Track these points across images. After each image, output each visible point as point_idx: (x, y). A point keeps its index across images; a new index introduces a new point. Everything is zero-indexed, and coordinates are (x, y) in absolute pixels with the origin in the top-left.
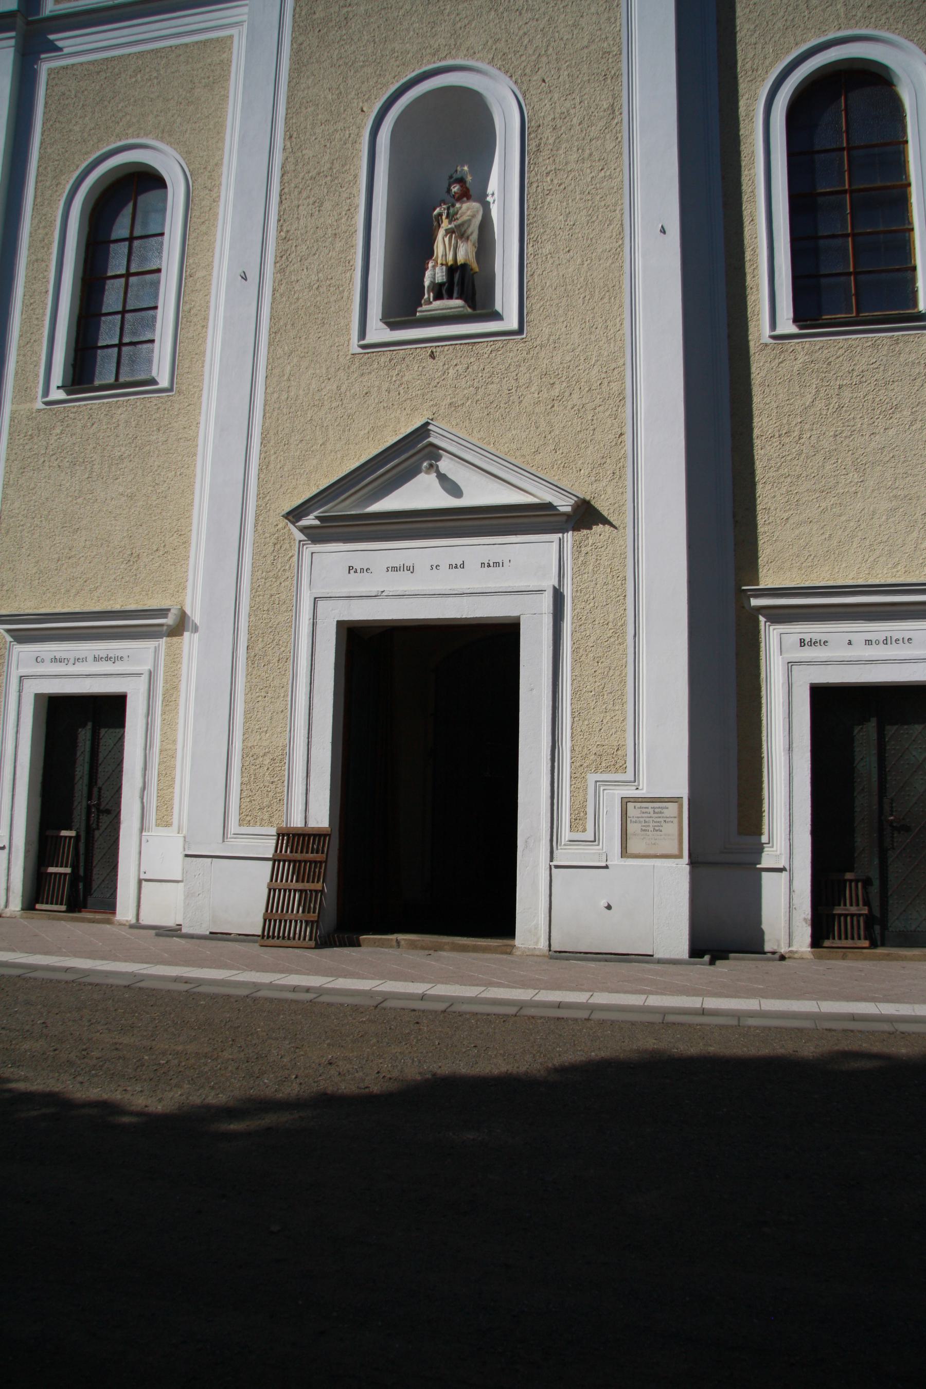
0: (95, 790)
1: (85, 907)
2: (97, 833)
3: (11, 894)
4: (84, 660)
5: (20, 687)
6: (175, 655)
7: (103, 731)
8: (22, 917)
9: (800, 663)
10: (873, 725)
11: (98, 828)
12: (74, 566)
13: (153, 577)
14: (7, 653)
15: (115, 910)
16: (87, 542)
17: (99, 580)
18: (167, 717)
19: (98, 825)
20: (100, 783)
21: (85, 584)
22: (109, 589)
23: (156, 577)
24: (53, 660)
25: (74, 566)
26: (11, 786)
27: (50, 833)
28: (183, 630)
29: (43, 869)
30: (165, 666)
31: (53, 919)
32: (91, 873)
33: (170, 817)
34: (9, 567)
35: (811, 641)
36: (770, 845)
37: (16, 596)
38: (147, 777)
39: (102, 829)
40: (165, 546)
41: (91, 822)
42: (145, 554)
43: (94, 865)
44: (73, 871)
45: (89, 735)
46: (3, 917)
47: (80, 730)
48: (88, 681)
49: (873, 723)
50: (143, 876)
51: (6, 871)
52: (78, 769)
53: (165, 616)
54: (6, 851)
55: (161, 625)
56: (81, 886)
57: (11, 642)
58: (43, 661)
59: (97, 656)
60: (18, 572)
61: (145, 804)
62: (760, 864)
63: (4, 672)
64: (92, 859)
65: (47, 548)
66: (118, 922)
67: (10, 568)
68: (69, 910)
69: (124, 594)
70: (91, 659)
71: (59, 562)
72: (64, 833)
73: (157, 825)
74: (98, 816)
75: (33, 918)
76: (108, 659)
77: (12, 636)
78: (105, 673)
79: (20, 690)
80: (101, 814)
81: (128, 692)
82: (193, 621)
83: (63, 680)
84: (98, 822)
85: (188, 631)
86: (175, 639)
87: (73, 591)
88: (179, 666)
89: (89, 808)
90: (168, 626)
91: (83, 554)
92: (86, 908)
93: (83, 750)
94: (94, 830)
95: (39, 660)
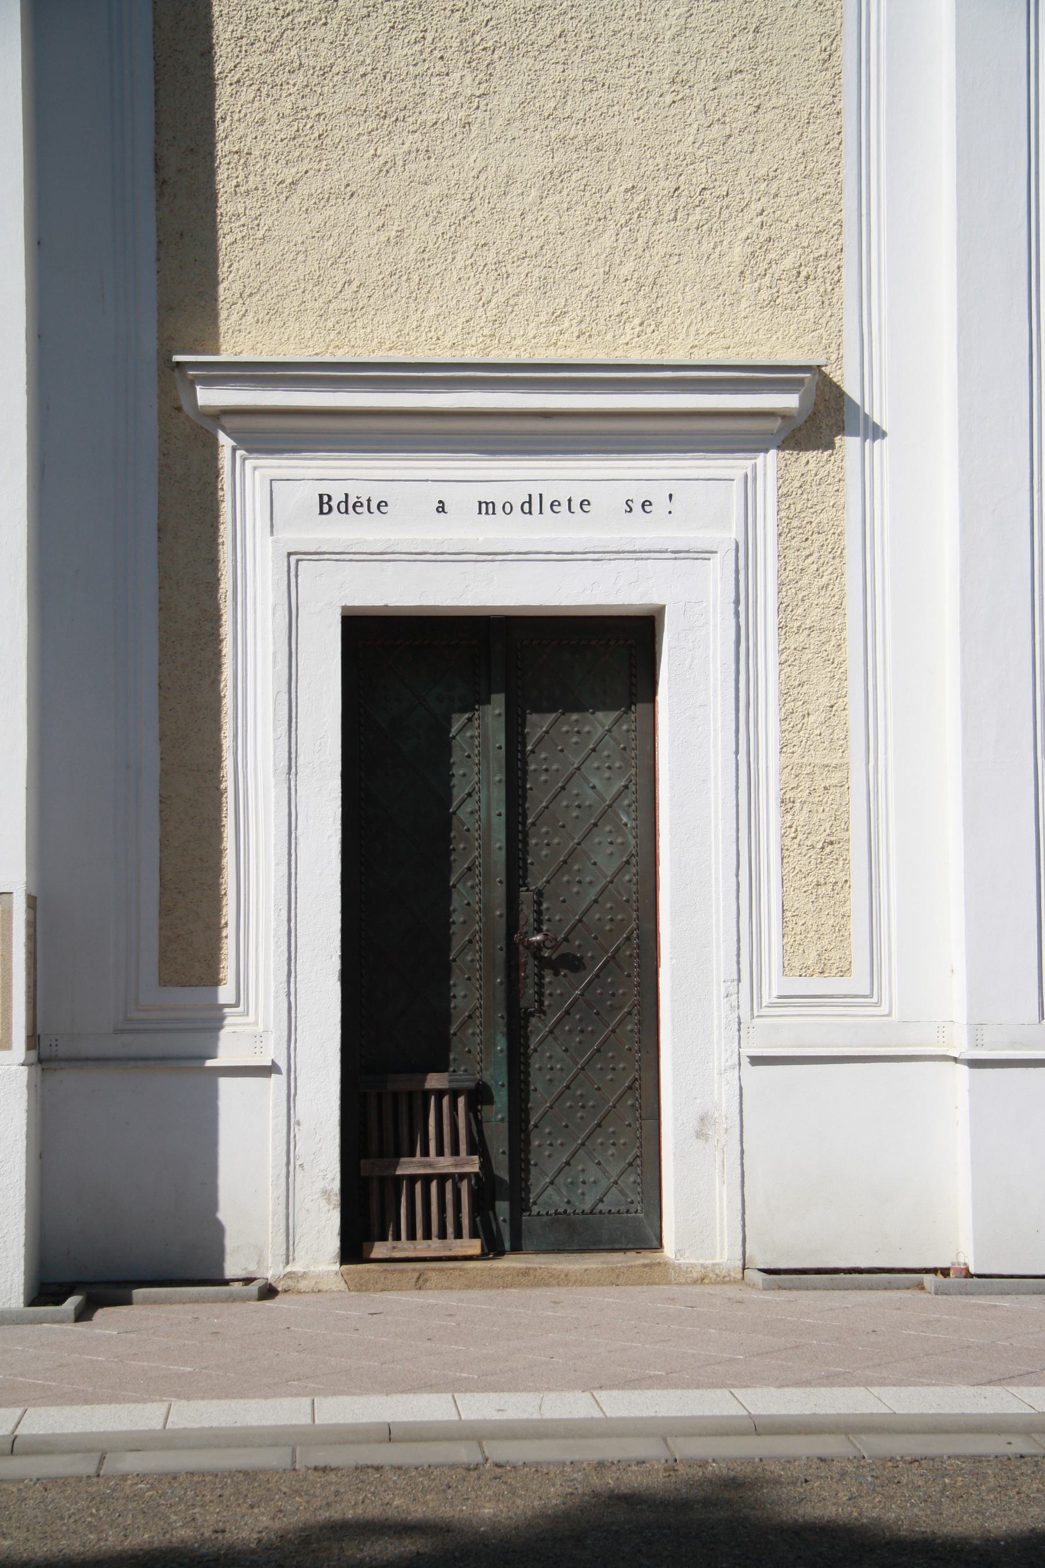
7: (538, 724)
20: (537, 879)
36: (241, 1009)
49: (495, 709)
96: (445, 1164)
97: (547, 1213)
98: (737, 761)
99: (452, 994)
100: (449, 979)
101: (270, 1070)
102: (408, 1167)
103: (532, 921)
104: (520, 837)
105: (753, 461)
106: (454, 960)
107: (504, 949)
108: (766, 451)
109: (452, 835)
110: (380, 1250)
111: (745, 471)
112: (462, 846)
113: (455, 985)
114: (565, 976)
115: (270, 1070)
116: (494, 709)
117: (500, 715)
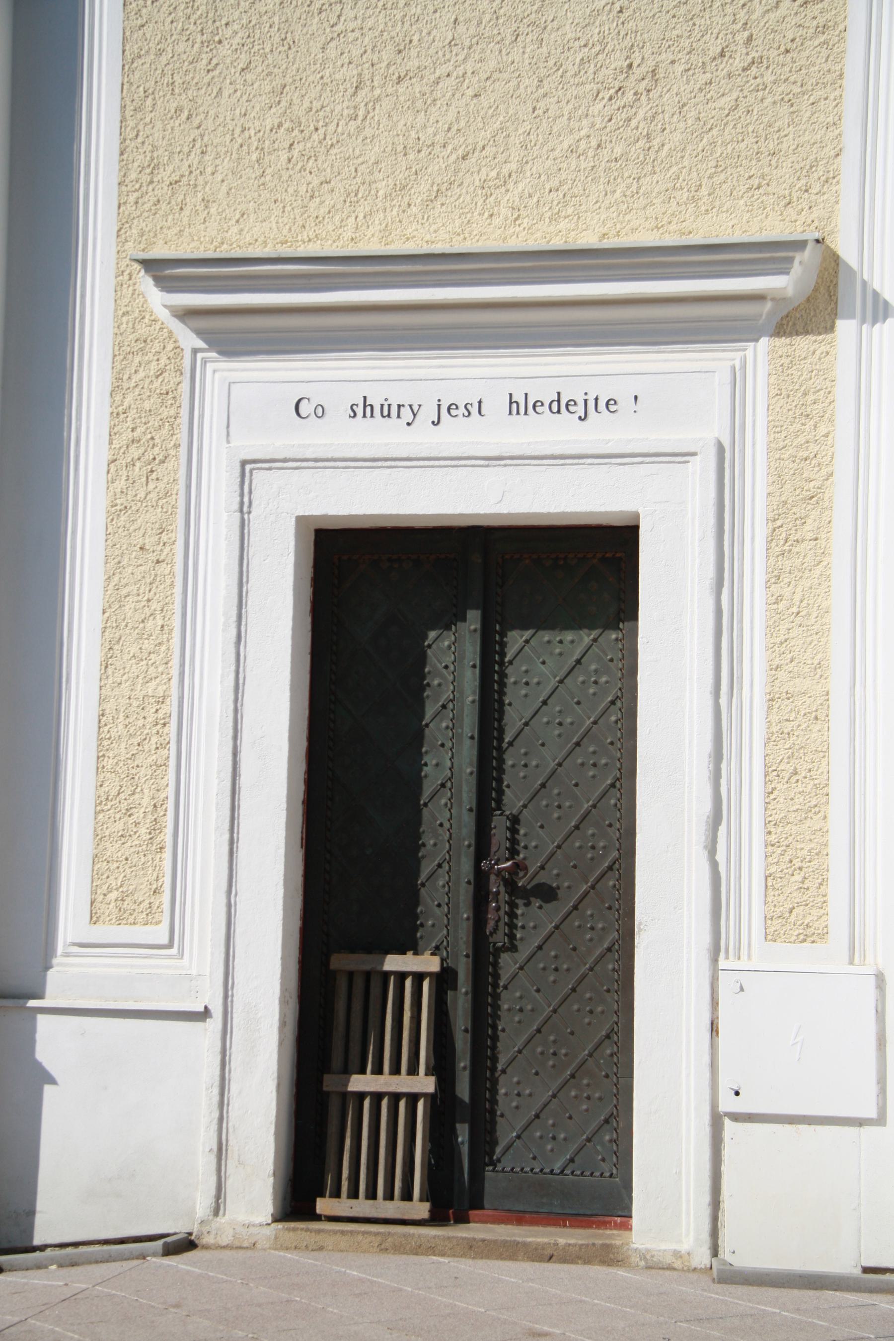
0: (499, 825)
1: (477, 1203)
2: (508, 964)
3: (231, 1166)
4: (474, 410)
5: (242, 495)
6: (805, 394)
7: (516, 639)
8: (276, 1241)
9: (269, 463)
10: (472, 627)
11: (513, 948)
12: (419, 104)
13: (713, 143)
14: (185, 387)
15: (630, 1210)
16: (461, 28)
17: (515, 154)
18: (787, 592)
19: (512, 937)
20: (513, 800)
21: (464, 165)
22: (554, 183)
23: (725, 144)
24: (359, 411)
25: (419, 104)
26: (228, 813)
27: (341, 962)
28: (834, 315)
29: (330, 1083)
30: (774, 427)
31: (399, 1249)
32: (494, 1091)
33: (815, 912)
34: (173, 105)
35: (559, 401)
36: (174, 951)
37: (206, 203)
38: (723, 781)
39: (524, 952)
40: (750, 39)
41: (491, 925)
42: (679, 68)
43: (500, 1067)
44: (440, 1083)
45: (471, 650)
46: (206, 1247)
47: (432, 634)
48: (494, 475)
49: (474, 619)
50: (728, 1104)
51: (216, 1091)
52: (430, 760)
53: (782, 267)
54: (214, 1024)
55: (757, 297)
56: (463, 1133)
57: (195, 351)
58: (321, 412)
59: (519, 398)
60: (209, 124)
61: (722, 869)
62: (40, 996)
63: (177, 446)
64: (494, 1048)
65: (315, 48)
66: (643, 1257)
67: (179, 110)
68: (437, 1218)
69: (610, 199)
70: (496, 405)
71: (362, 93)
72: (393, 963)
73: (770, 937)
74: (513, 905)
75: (321, 1248)
76: (559, 405)
77: (199, 333)
78: (557, 451)
79: (242, 503)
80: (520, 902)
81: (641, 511)
82: (864, 283)
83: (401, 475)
84: (512, 926)
85: (851, 316)
86: (803, 344)
87: (422, 189)
88: (822, 429)
89: (480, 879)
90: (779, 300)
91: (449, 67)
92: (481, 1207)
93: (447, 695)
94: (498, 951)
95: (304, 408)
96: (403, 1084)
97: (512, 1169)
98: (714, 865)
99: (423, 762)
100: (422, 746)
101: (205, 1015)
102: (359, 1083)
103: (503, 848)
104: (495, 734)
105: (741, 353)
106: (426, 805)
107: (471, 955)
108: (756, 340)
109: (427, 670)
110: (323, 1205)
111: (732, 363)
112: (436, 682)
113: (426, 752)
114: (540, 907)
115: (205, 1015)
116: (470, 625)
117: (475, 630)
